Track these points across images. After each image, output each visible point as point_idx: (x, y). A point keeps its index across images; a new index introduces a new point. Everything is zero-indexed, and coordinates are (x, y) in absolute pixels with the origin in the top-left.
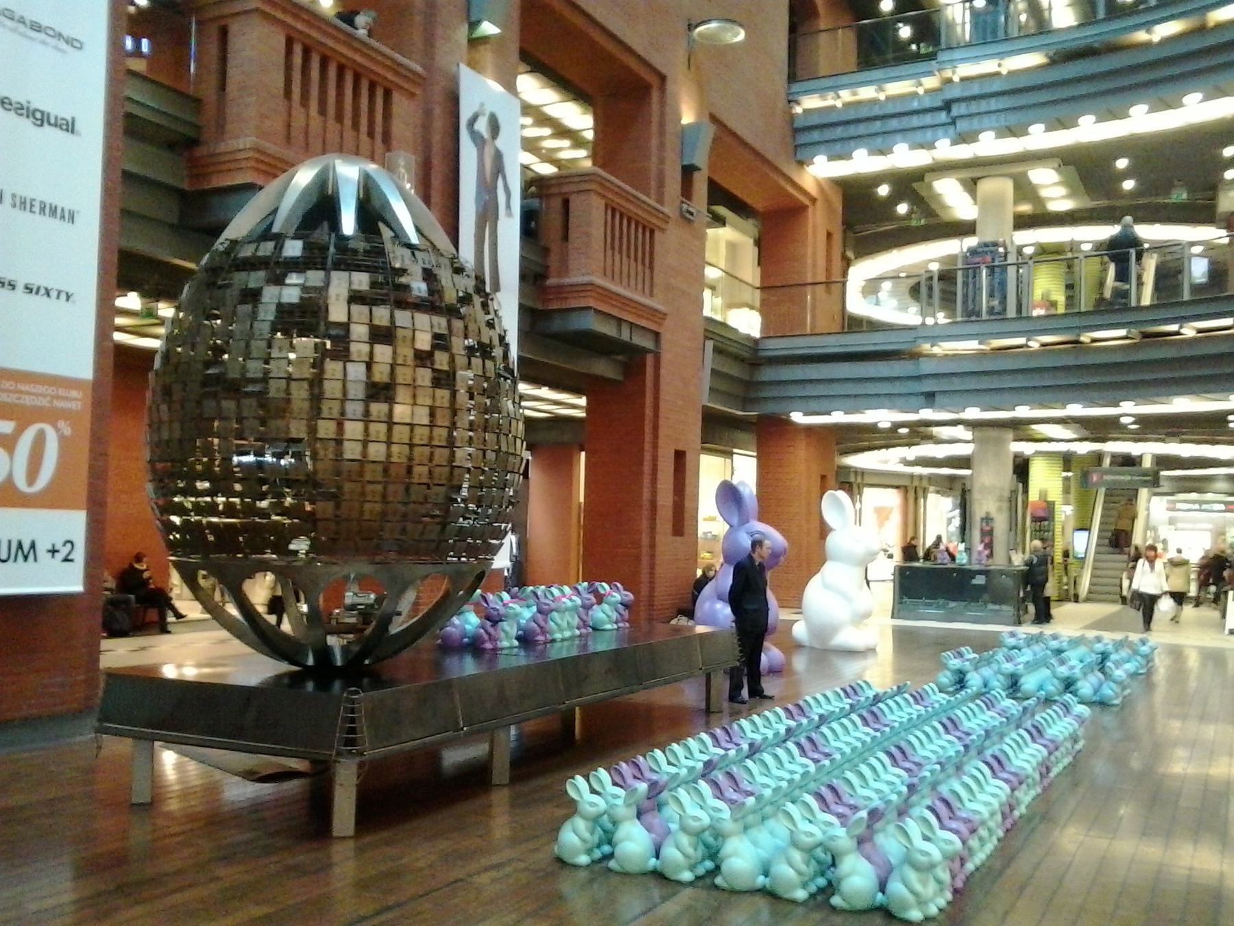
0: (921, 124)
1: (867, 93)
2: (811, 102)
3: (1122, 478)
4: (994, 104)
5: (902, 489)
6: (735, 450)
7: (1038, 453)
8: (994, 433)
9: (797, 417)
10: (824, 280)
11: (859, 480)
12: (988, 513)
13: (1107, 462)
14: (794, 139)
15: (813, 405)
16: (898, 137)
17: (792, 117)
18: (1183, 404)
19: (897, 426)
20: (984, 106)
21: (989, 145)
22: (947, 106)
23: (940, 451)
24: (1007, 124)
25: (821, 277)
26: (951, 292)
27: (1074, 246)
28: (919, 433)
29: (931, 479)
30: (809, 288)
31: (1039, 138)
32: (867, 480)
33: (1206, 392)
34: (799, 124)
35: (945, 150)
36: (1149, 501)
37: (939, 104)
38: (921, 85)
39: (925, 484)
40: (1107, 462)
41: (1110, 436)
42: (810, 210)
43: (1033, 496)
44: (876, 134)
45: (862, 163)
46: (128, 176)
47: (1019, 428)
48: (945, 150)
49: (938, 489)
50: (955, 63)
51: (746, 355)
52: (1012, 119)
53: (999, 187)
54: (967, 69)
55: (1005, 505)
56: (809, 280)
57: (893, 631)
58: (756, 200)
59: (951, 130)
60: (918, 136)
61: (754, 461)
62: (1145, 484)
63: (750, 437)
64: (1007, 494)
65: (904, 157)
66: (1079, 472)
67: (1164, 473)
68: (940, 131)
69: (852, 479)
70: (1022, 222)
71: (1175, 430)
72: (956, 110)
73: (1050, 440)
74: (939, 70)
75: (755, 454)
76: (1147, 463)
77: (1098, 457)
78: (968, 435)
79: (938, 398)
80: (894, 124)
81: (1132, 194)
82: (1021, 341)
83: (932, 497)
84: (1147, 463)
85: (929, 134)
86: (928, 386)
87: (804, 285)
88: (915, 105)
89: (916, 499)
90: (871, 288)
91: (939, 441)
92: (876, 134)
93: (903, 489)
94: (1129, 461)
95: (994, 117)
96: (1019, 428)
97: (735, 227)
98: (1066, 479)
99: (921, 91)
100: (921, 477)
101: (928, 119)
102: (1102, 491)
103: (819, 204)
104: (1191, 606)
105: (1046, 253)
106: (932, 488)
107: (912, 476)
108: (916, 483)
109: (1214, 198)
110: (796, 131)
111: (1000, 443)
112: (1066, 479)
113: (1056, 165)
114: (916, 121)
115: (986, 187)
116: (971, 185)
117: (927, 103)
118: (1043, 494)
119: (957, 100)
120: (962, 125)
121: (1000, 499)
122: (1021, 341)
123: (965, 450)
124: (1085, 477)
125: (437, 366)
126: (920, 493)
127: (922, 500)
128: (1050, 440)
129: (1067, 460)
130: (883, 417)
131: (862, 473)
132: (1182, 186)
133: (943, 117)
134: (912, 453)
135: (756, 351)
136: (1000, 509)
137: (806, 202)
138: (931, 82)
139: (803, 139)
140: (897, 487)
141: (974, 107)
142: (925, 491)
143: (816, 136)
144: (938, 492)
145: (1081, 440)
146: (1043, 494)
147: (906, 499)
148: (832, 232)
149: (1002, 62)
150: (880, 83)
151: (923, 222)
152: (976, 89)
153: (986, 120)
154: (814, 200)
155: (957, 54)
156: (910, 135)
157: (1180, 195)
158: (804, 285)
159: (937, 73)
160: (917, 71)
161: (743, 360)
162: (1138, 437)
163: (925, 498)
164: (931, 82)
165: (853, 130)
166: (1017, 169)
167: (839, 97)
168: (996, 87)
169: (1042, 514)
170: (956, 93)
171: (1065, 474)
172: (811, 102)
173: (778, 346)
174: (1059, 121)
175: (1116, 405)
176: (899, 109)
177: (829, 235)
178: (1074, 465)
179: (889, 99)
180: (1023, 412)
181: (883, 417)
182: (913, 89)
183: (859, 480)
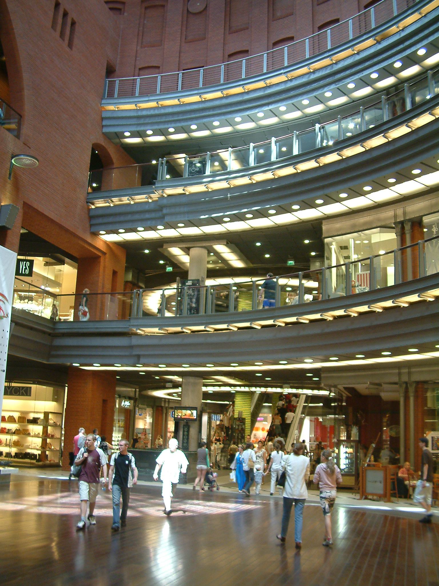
1: (125, 200)
2: (100, 203)
4: (182, 209)
10: (110, 292)
14: (90, 222)
15: (107, 361)
17: (89, 210)
20: (177, 210)
30: (99, 296)
34: (92, 213)
42: (102, 259)
46: (216, 297)
54: (170, 191)
56: (100, 291)
69: (163, 405)
70: (212, 274)
72: (165, 211)
82: (202, 328)
86: (136, 352)
87: (98, 294)
97: (69, 264)
101: (153, 215)
103: (107, 255)
110: (91, 218)
113: (225, 243)
114: (147, 216)
115: (193, 251)
116: (187, 250)
118: (240, 413)
119: (166, 206)
122: (202, 328)
125: (178, 485)
132: (292, 258)
137: (100, 254)
139: (94, 222)
141: (173, 210)
143: (100, 221)
146: (240, 413)
148: (116, 270)
154: (104, 254)
159: (156, 192)
164: (155, 196)
170: (165, 202)
172: (100, 203)
177: (115, 273)
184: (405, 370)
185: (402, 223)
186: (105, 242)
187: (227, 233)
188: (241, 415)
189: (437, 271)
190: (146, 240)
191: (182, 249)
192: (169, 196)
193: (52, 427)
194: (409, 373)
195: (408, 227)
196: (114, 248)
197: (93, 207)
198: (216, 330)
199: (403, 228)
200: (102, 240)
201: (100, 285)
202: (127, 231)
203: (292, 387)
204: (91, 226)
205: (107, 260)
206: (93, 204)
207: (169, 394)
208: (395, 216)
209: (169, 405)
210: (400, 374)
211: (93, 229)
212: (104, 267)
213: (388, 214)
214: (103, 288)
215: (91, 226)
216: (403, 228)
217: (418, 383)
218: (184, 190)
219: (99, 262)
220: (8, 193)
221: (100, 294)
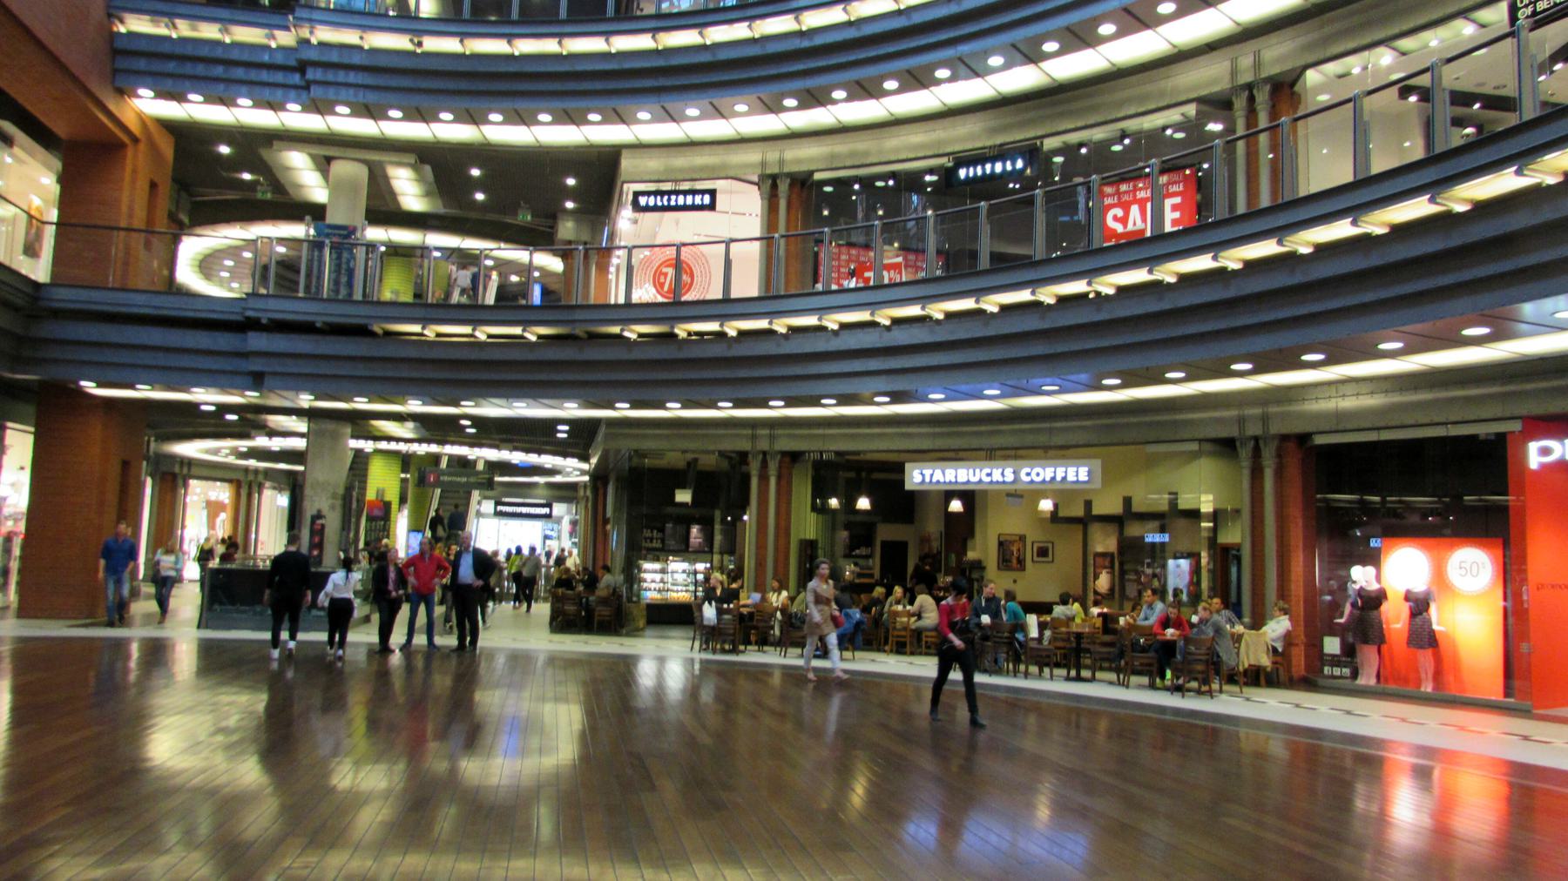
0: (271, 80)
1: (209, 31)
3: (459, 479)
4: (352, 77)
5: (234, 484)
6: (10, 424)
7: (378, 452)
8: (330, 426)
9: (89, 386)
10: (143, 227)
11: (185, 471)
12: (319, 511)
13: (444, 464)
14: (113, 64)
15: (112, 375)
16: (244, 89)
18: (523, 409)
19: (223, 409)
20: (341, 76)
21: (345, 122)
22: (302, 67)
23: (276, 444)
24: (365, 101)
25: (139, 223)
26: (291, 281)
27: (424, 250)
28: (250, 421)
29: (268, 473)
31: (398, 128)
32: (195, 471)
33: (543, 397)
34: (119, 44)
35: (295, 118)
36: (479, 503)
37: (293, 63)
38: (274, 37)
39: (261, 478)
40: (444, 464)
41: (449, 439)
42: (130, 153)
43: (371, 495)
44: (217, 80)
45: (198, 110)
47: (359, 422)
48: (295, 118)
49: (276, 485)
50: (313, 24)
51: (19, 302)
52: (371, 98)
53: (349, 169)
54: (325, 34)
55: (339, 503)
56: (123, 224)
57: (199, 645)
58: (61, 129)
59: (304, 94)
60: (267, 93)
61: (31, 439)
62: (479, 486)
63: (31, 410)
64: (341, 491)
65: (247, 114)
66: (416, 475)
67: (498, 479)
68: (293, 93)
69: (177, 469)
71: (509, 437)
72: (311, 74)
73: (389, 439)
74: (295, 26)
75: (32, 429)
76: (480, 466)
77: (436, 458)
78: (301, 426)
79: (268, 381)
80: (240, 73)
81: (482, 206)
83: (268, 493)
84: (480, 466)
85: (279, 93)
86: (256, 365)
88: (266, 58)
89: (250, 496)
90: (207, 265)
91: (272, 433)
92: (217, 80)
93: (237, 484)
94: (463, 464)
95: (351, 91)
96: (359, 422)
98: (404, 481)
99: (274, 45)
100: (256, 471)
101: (279, 77)
102: (438, 491)
103: (142, 146)
104: (507, 606)
105: (397, 251)
106: (268, 484)
107: (246, 470)
108: (251, 477)
109: (553, 227)
111: (336, 438)
112: (404, 481)
114: (265, 76)
115: (341, 168)
116: (323, 165)
117: (279, 59)
118: (380, 492)
119: (316, 64)
120: (316, 92)
121: (334, 496)
123: (300, 444)
124: (422, 481)
126: (256, 488)
127: (257, 495)
128: (389, 439)
129: (406, 461)
130: (206, 397)
131: (188, 463)
133: (296, 78)
134: (243, 445)
135: (36, 299)
136: (333, 507)
138: (285, 38)
139: (123, 63)
140: (229, 481)
142: (261, 487)
144: (274, 488)
145: (419, 441)
146: (380, 492)
147: (238, 495)
148: (156, 180)
149: (365, 36)
150: (225, 22)
151: (269, 196)
152: (334, 57)
153: (344, 93)
154: (135, 140)
155: (316, 15)
156: (257, 89)
157: (526, 217)
158: (112, 228)
159: (293, 29)
160: (272, 22)
161: (17, 309)
162: (474, 442)
163: (260, 494)
164: (285, 38)
165: (188, 68)
166: (374, 156)
167: (175, 27)
168: (356, 59)
169: (377, 513)
170: (313, 55)
171: (403, 476)
173: (66, 297)
174: (418, 110)
175: (456, 404)
176: (246, 57)
177: (153, 186)
178: (413, 468)
179: (235, 45)
180: (361, 404)
181: (206, 397)
182: (264, 41)
183: (185, 471)
184: (766, 432)
185: (774, 178)
186: (142, 118)
187: (434, 143)
188: (383, 495)
189: (52, 223)
190: (242, 127)
191: (314, 157)
192: (322, 44)
193: (820, 516)
194: (772, 438)
195: (783, 187)
196: (152, 127)
197: (123, 30)
198: (438, 335)
199: (774, 186)
200: (133, 109)
201: (124, 209)
202: (408, 117)
203: (527, 451)
204: (115, 71)
205: (141, 156)
206: (122, 22)
207: (208, 451)
208: (763, 164)
209: (189, 470)
210: (754, 437)
211: (120, 83)
212: (134, 171)
213: (752, 156)
214: (131, 216)
215: (115, 71)
216: (774, 186)
217: (784, 454)
218: (361, 38)
219: (124, 157)
220: (1170, 84)
221: (123, 229)
